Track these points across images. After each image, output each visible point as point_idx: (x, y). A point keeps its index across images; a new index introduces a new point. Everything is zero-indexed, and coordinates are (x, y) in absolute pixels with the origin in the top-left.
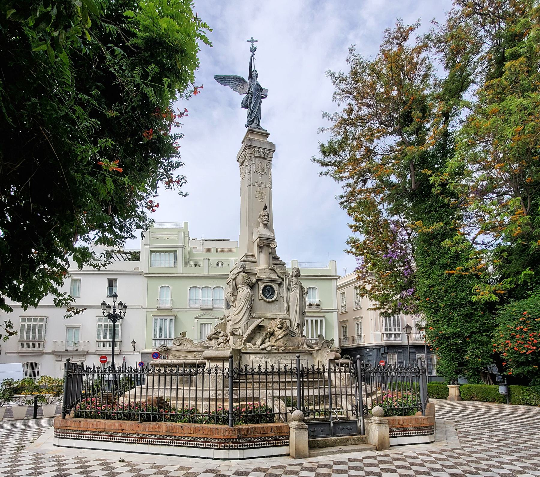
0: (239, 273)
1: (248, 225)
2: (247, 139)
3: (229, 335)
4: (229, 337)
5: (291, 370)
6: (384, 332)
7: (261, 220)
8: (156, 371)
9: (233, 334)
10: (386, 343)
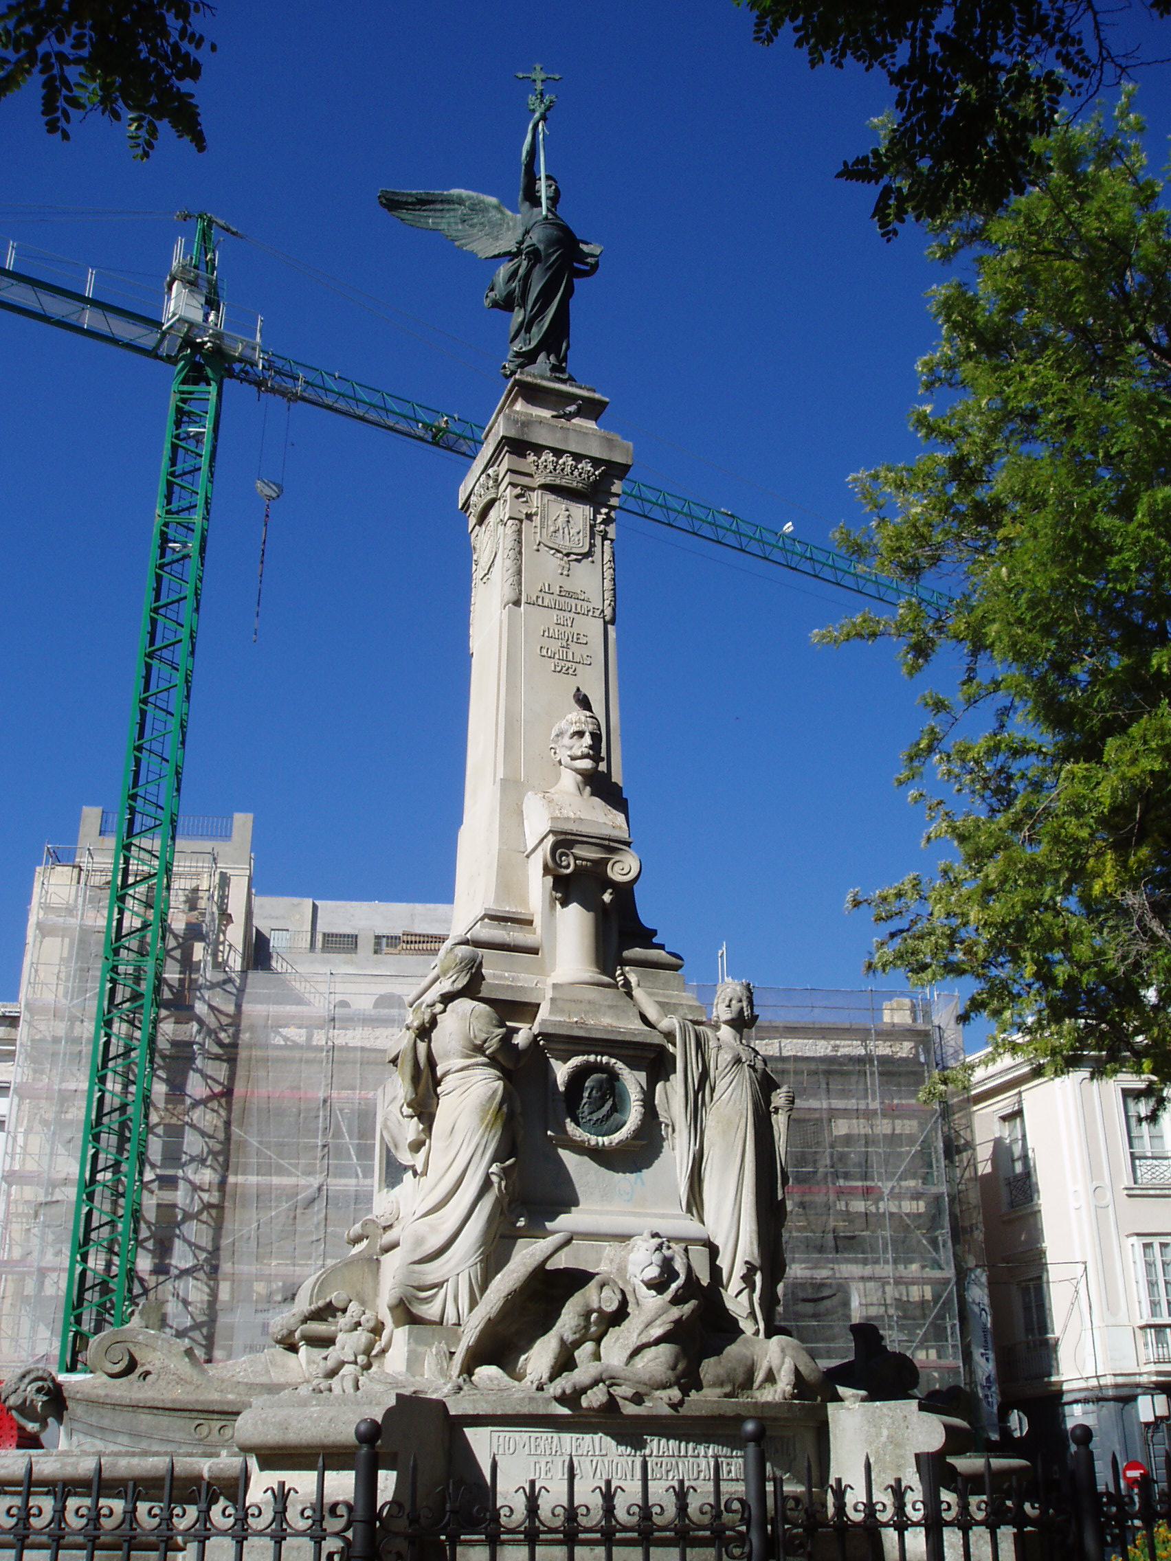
0: (447, 999)
1: (500, 775)
2: (508, 418)
3: (387, 1317)
4: (386, 1333)
5: (718, 1515)
6: (1147, 1319)
7: (564, 755)
8: (74, 1522)
9: (406, 1313)
10: (1159, 1373)
